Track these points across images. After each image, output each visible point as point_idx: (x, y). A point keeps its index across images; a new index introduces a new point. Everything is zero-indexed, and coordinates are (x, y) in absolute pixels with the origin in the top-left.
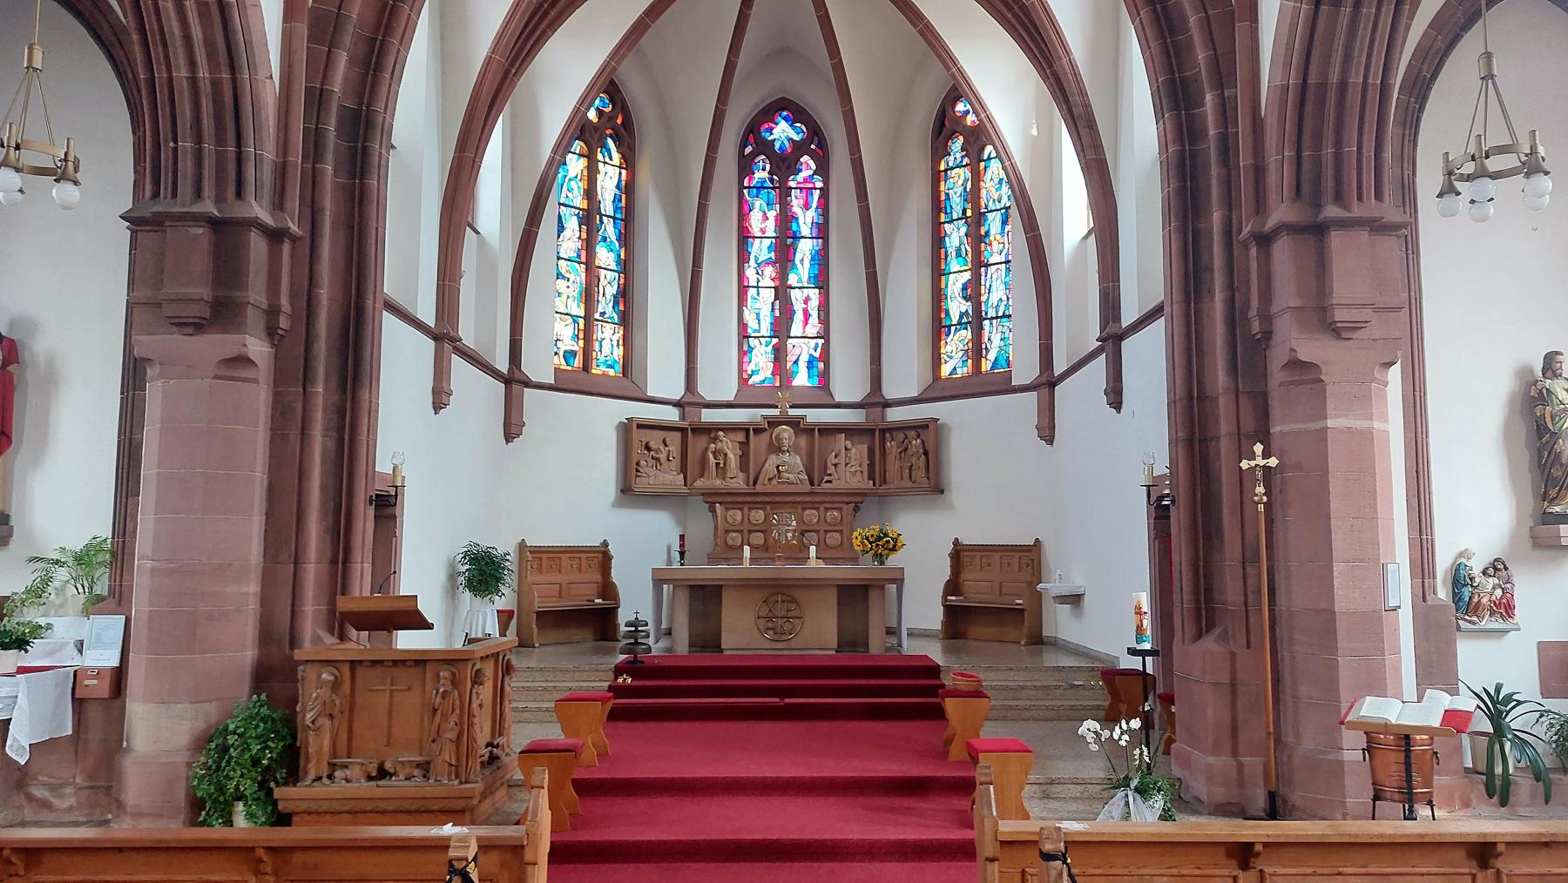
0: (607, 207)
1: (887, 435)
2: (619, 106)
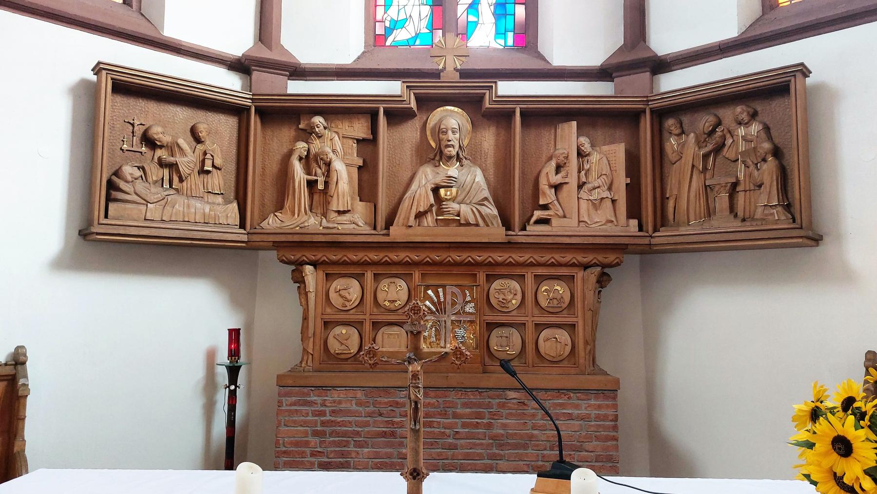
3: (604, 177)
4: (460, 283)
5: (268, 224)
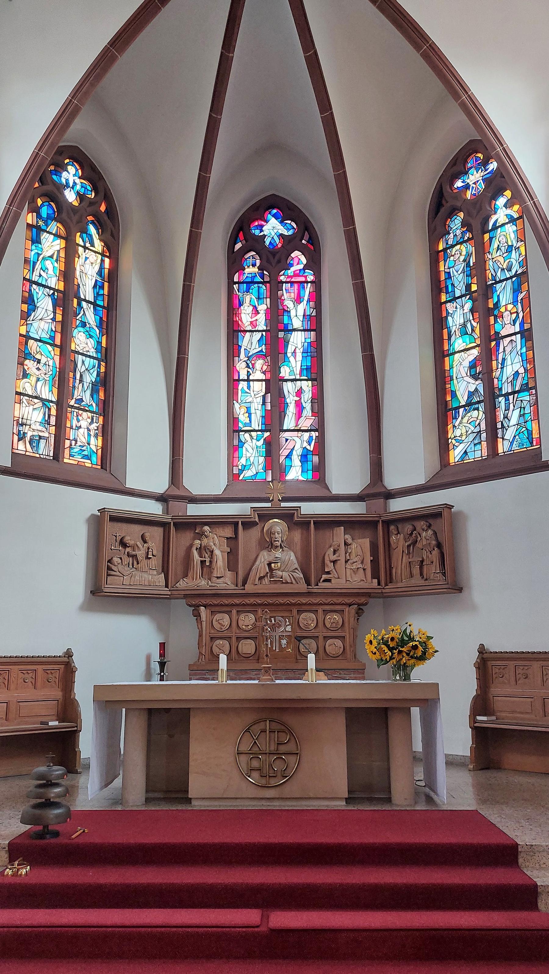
0: (87, 292)
1: (392, 527)
2: (102, 194)
3: (359, 556)
4: (283, 615)
5: (180, 585)
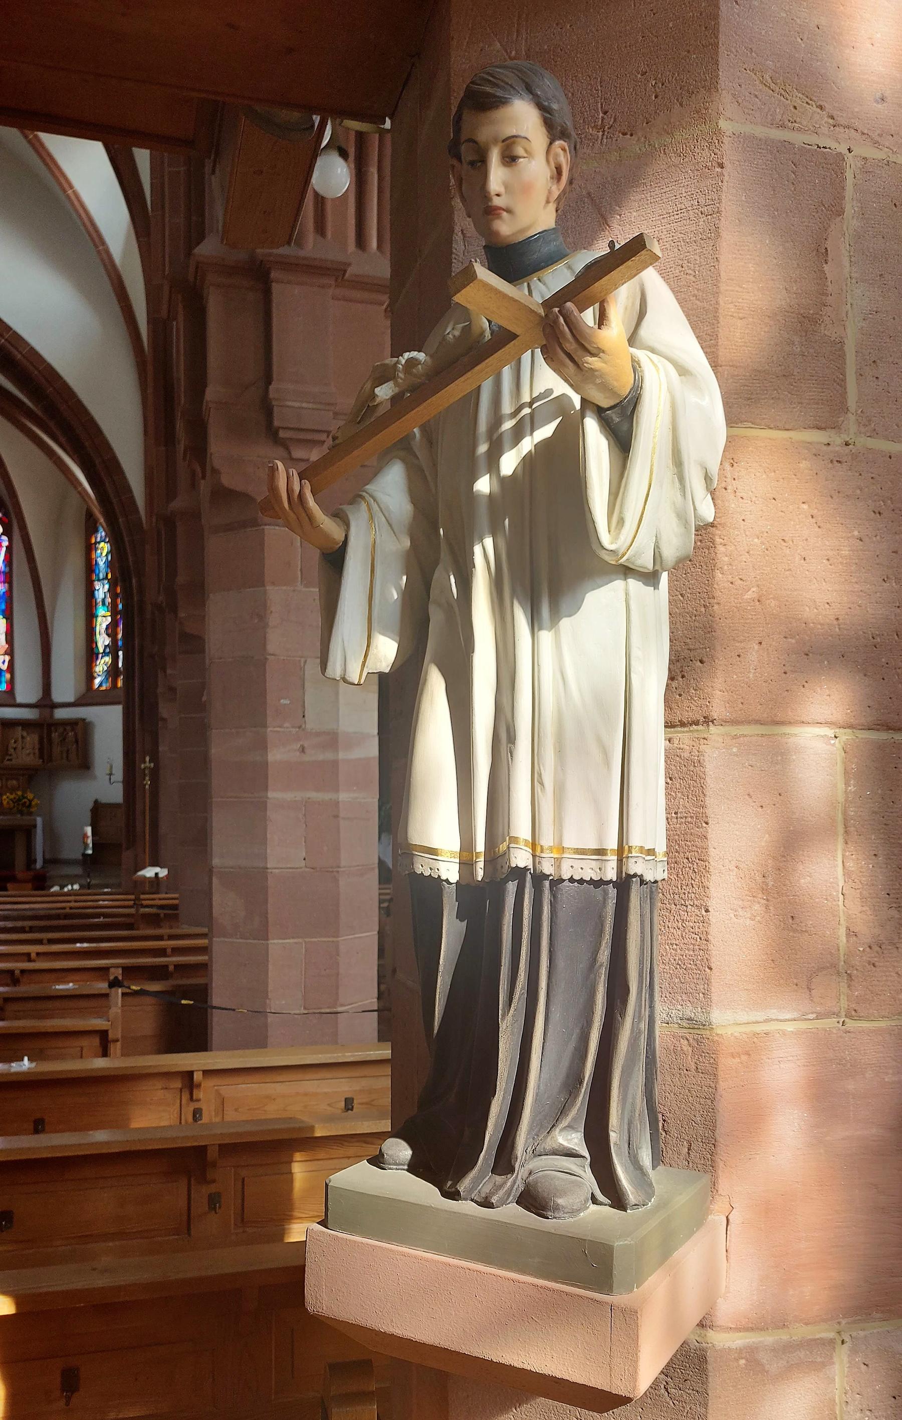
1: (53, 728)
